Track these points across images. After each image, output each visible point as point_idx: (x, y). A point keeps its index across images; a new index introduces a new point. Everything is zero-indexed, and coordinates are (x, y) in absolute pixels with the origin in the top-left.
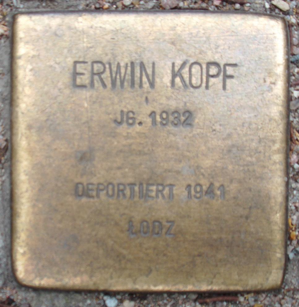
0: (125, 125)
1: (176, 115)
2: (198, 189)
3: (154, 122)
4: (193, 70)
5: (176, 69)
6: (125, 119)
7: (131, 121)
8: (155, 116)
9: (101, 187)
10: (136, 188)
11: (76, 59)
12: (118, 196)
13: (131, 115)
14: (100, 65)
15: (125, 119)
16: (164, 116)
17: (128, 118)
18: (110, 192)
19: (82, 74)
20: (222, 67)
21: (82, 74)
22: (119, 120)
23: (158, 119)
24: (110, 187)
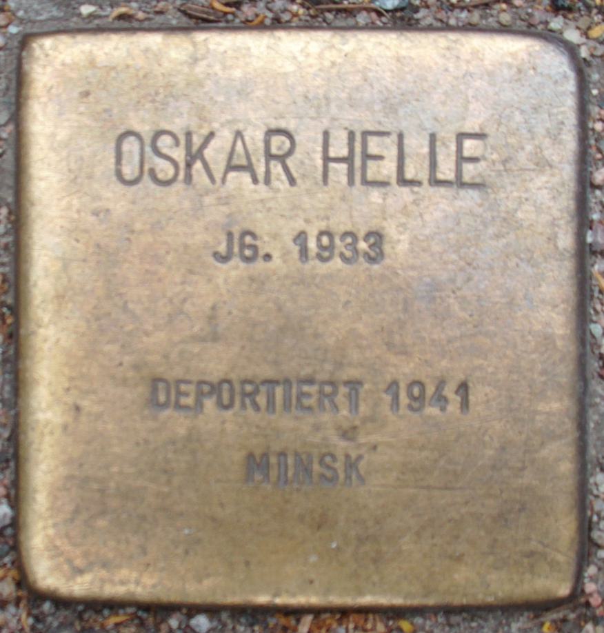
0: (236, 261)
1: (349, 240)
2: (416, 391)
3: (304, 252)
4: (126, 147)
5: (195, 148)
6: (236, 249)
7: (248, 253)
8: (306, 240)
9: (206, 388)
10: (279, 391)
11: (274, 124)
12: (243, 406)
13: (248, 239)
14: (283, 138)
15: (236, 249)
16: (325, 240)
17: (243, 246)
18: (226, 401)
19: (380, 158)
20: (147, 141)
21: (380, 158)
22: (222, 248)
23: (312, 245)
24: (226, 386)
